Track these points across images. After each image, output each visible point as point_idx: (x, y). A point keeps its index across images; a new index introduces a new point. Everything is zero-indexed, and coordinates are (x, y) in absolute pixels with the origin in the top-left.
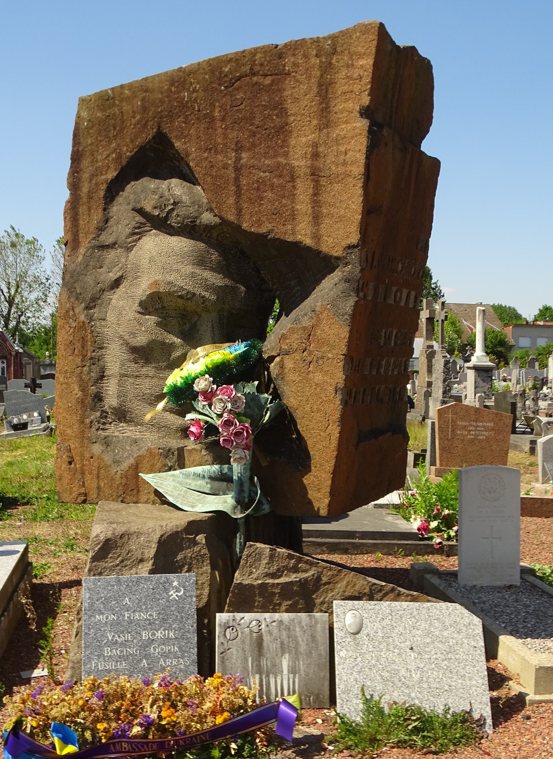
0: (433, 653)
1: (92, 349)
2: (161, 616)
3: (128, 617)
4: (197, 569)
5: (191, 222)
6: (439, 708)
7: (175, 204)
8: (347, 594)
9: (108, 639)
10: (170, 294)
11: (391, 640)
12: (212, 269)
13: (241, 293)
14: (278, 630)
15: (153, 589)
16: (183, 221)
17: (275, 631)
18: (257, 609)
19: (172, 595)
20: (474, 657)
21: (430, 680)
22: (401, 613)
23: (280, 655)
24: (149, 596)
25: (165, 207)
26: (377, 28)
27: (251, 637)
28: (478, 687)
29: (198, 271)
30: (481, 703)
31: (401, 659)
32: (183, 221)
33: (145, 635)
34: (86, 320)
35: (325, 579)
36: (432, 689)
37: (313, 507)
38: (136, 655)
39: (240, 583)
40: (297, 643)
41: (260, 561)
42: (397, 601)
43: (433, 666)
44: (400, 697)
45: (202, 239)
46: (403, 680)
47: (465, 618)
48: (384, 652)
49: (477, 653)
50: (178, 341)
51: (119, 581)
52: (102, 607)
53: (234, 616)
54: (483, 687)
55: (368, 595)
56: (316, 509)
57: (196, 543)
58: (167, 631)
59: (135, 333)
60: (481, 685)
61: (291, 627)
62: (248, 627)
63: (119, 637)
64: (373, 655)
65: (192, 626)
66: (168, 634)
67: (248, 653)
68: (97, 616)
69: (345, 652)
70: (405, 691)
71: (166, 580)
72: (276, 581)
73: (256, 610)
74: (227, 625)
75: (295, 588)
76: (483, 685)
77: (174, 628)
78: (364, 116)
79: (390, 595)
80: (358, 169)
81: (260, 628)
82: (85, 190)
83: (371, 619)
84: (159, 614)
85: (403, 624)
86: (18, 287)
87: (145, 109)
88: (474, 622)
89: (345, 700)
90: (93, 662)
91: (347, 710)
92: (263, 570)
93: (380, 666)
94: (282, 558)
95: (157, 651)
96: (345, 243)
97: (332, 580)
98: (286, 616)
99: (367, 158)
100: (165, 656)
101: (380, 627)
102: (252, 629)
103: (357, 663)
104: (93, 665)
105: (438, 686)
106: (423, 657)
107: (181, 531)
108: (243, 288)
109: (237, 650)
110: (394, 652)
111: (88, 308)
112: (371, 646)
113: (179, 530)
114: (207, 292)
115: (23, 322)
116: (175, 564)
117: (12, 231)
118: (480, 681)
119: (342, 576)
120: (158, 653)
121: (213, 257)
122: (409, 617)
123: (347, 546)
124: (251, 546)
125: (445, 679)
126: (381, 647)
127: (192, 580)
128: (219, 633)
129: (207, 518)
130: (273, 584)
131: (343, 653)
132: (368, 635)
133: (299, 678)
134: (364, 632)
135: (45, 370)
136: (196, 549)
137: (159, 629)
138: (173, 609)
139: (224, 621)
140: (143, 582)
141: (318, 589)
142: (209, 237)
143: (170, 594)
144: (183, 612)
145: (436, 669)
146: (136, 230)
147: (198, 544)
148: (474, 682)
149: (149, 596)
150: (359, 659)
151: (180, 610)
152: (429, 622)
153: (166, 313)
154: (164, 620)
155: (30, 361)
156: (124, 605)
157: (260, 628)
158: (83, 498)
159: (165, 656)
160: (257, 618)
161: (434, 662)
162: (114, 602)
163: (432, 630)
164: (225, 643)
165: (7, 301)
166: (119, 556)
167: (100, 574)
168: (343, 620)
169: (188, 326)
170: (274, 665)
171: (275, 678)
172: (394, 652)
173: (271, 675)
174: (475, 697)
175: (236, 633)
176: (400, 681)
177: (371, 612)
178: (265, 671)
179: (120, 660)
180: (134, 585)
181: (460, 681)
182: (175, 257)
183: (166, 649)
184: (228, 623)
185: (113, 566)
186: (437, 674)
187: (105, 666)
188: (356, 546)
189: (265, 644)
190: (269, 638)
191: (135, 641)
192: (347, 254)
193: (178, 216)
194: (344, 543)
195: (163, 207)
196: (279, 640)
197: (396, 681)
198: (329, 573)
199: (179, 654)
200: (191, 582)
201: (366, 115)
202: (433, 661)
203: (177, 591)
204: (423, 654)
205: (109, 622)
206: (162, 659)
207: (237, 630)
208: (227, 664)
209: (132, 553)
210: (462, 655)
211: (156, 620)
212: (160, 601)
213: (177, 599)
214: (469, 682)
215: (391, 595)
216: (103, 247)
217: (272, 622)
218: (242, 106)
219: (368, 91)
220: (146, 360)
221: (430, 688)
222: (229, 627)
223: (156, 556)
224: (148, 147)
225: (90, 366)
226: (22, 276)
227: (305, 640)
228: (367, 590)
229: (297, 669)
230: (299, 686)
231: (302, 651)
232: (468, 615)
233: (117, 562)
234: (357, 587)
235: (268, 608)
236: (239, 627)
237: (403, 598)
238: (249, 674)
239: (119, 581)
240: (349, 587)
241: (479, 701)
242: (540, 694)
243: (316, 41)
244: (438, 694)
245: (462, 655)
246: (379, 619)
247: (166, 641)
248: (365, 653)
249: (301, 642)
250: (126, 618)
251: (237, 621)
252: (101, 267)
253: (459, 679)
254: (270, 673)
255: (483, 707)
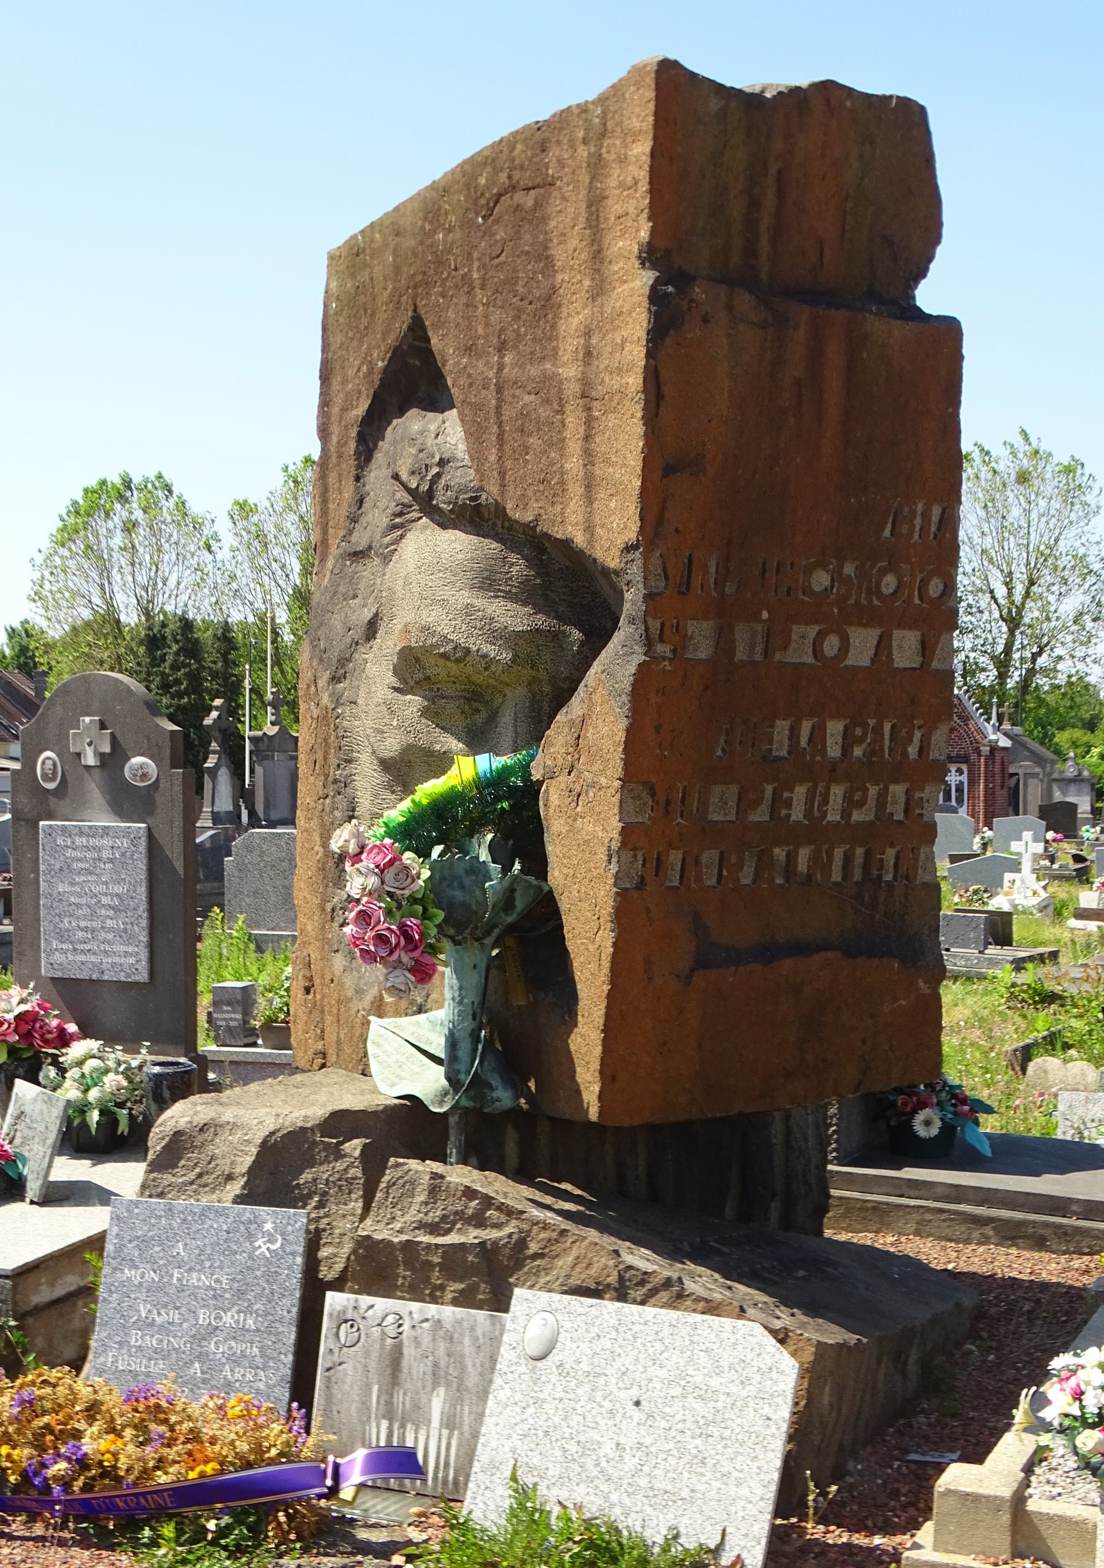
0: (678, 1418)
1: (337, 761)
2: (236, 1285)
3: (179, 1280)
4: (337, 1204)
5: (471, 499)
6: (658, 1533)
7: (442, 463)
8: (574, 1282)
9: (140, 1316)
10: (427, 650)
11: (601, 1381)
12: (509, 596)
13: (572, 644)
14: (431, 1338)
15: (228, 1232)
16: (457, 498)
17: (426, 1340)
18: (402, 1292)
19: (260, 1247)
20: (761, 1439)
21: (657, 1472)
22: (636, 1328)
23: (429, 1388)
24: (219, 1244)
25: (427, 471)
26: (653, 75)
27: (382, 1345)
28: (750, 1502)
29: (479, 602)
30: (746, 1535)
31: (611, 1423)
32: (457, 498)
33: (204, 1317)
34: (329, 705)
35: (533, 1247)
36: (656, 1492)
37: (582, 1101)
38: (184, 1353)
39: (368, 1237)
40: (463, 1369)
41: (413, 1196)
42: (675, 1308)
43: (671, 1445)
44: (588, 1498)
45: (497, 534)
46: (604, 1464)
47: (764, 1355)
48: (581, 1403)
49: (768, 1432)
50: (454, 744)
51: (170, 1210)
52: (136, 1254)
53: (356, 1300)
54: (762, 1504)
55: (616, 1290)
56: (585, 1105)
57: (339, 1156)
58: (242, 1315)
59: (383, 732)
60: (758, 1498)
61: (456, 1336)
62: (379, 1325)
63: (159, 1314)
64: (560, 1406)
65: (289, 1312)
66: (245, 1320)
67: (374, 1377)
68: (126, 1271)
69: (509, 1393)
70: (602, 1487)
71: (252, 1217)
72: (440, 1240)
73: (399, 1294)
74: (343, 1317)
75: (470, 1258)
76: (762, 1499)
77: (256, 1312)
78: (647, 264)
79: (663, 1293)
80: (634, 381)
81: (400, 1330)
82: (335, 439)
83: (576, 1333)
84: (233, 1280)
85: (636, 1352)
86: (1032, 583)
87: (397, 270)
88: (782, 1367)
89: (483, 1487)
90: (111, 1354)
91: (481, 1505)
92: (415, 1216)
93: (568, 1430)
94: (454, 1195)
95: (221, 1350)
96: (620, 542)
97: (547, 1250)
98: (448, 1313)
99: (649, 355)
100: (235, 1360)
101: (589, 1351)
102: (386, 1330)
103: (524, 1417)
104: (110, 1360)
105: (669, 1488)
106: (657, 1424)
107: (312, 1129)
108: (576, 634)
109: (355, 1368)
110: (601, 1407)
111: (335, 679)
112: (561, 1388)
113: (309, 1125)
114: (494, 644)
115: (1045, 671)
116: (293, 1192)
117: (1022, 442)
118: (759, 1491)
119: (568, 1244)
120: (223, 1353)
121: (514, 569)
122: (650, 1338)
123: (1041, 1232)
124: (397, 1165)
125: (686, 1475)
126: (580, 1392)
127: (299, 1223)
128: (328, 1329)
129: (381, 1108)
130: (429, 1246)
131: (502, 1395)
132: (561, 1365)
133: (459, 1439)
134: (554, 1358)
135: (1064, 793)
136: (340, 1165)
137: (229, 1309)
138: (259, 1273)
139: (338, 1308)
140: (212, 1216)
141: (518, 1265)
142: (508, 529)
143: (257, 1244)
144: (275, 1281)
145: (675, 1452)
146: (397, 520)
147: (345, 1156)
148: (745, 1491)
149: (219, 1244)
150: (531, 1410)
151: (272, 1277)
152: (688, 1354)
153: (438, 689)
154: (240, 1293)
155: (1037, 770)
156: (174, 1257)
157: (400, 1330)
158: (320, 1061)
159: (235, 1360)
160: (397, 1309)
161: (674, 1437)
162: (157, 1249)
163: (690, 1371)
164: (336, 1350)
165: (1003, 620)
166: (196, 1165)
167: (161, 1195)
168: (522, 1330)
169: (480, 719)
170: (417, 1407)
171: (416, 1432)
172: (601, 1407)
173: (409, 1426)
174: (737, 1522)
175: (356, 1334)
176: (597, 1465)
177: (579, 1319)
178: (400, 1416)
179: (156, 1356)
180: (195, 1221)
181: (716, 1484)
182: (441, 575)
183: (237, 1347)
184: (344, 1312)
185: (184, 1184)
186: (673, 1463)
187: (129, 1365)
188: (1065, 1234)
189: (405, 1363)
190: (413, 1352)
191: (185, 1325)
192: (627, 563)
193: (447, 487)
194: (1034, 1222)
195: (424, 470)
196: (431, 1358)
197: (590, 1463)
198: (542, 1236)
199: (259, 1361)
200: (297, 1226)
201: (651, 262)
202: (673, 1434)
203: (269, 1241)
204: (658, 1418)
205: (145, 1285)
206: (227, 1367)
207: (359, 1329)
208: (335, 1392)
209: (218, 1162)
210: (736, 1431)
211: (225, 1291)
212: (238, 1257)
213: (268, 1255)
214: (734, 1488)
215: (664, 1296)
216: (358, 555)
217: (423, 1321)
218: (502, 258)
219: (646, 211)
220: (404, 786)
221: (652, 1488)
222: (346, 1321)
223: (253, 1171)
224: (405, 348)
225: (334, 797)
226: (1047, 555)
227: (478, 1365)
228: (613, 1279)
229: (458, 1419)
230: (457, 1455)
231: (470, 1385)
232: (774, 1350)
233: (192, 1175)
234: (594, 1270)
235: (422, 1292)
236: (364, 1322)
237: (689, 1303)
238: (370, 1418)
239: (170, 1210)
240: (578, 1269)
241: (743, 1532)
242: (947, 1551)
243: (583, 109)
244: (664, 1503)
245: (736, 1431)
246: (592, 1335)
247: (238, 1333)
248: (544, 1400)
249: (470, 1369)
250: (175, 1281)
251: (362, 1311)
252: (355, 596)
253: (717, 1479)
254: (408, 1421)
255: (749, 1545)
